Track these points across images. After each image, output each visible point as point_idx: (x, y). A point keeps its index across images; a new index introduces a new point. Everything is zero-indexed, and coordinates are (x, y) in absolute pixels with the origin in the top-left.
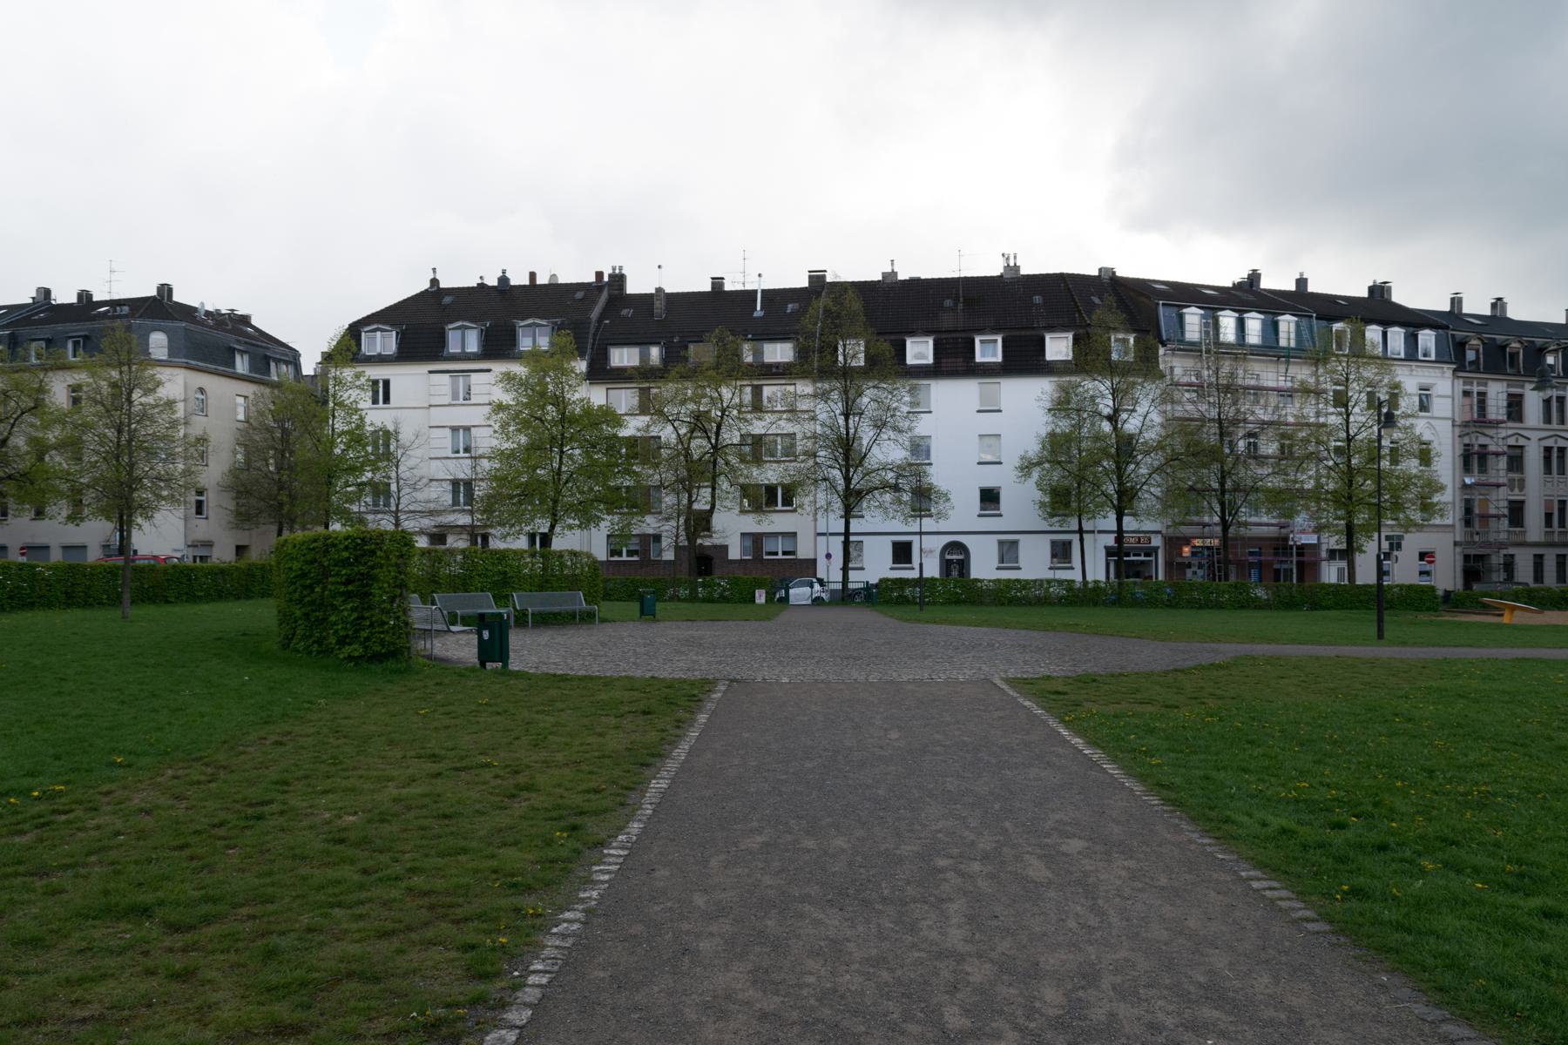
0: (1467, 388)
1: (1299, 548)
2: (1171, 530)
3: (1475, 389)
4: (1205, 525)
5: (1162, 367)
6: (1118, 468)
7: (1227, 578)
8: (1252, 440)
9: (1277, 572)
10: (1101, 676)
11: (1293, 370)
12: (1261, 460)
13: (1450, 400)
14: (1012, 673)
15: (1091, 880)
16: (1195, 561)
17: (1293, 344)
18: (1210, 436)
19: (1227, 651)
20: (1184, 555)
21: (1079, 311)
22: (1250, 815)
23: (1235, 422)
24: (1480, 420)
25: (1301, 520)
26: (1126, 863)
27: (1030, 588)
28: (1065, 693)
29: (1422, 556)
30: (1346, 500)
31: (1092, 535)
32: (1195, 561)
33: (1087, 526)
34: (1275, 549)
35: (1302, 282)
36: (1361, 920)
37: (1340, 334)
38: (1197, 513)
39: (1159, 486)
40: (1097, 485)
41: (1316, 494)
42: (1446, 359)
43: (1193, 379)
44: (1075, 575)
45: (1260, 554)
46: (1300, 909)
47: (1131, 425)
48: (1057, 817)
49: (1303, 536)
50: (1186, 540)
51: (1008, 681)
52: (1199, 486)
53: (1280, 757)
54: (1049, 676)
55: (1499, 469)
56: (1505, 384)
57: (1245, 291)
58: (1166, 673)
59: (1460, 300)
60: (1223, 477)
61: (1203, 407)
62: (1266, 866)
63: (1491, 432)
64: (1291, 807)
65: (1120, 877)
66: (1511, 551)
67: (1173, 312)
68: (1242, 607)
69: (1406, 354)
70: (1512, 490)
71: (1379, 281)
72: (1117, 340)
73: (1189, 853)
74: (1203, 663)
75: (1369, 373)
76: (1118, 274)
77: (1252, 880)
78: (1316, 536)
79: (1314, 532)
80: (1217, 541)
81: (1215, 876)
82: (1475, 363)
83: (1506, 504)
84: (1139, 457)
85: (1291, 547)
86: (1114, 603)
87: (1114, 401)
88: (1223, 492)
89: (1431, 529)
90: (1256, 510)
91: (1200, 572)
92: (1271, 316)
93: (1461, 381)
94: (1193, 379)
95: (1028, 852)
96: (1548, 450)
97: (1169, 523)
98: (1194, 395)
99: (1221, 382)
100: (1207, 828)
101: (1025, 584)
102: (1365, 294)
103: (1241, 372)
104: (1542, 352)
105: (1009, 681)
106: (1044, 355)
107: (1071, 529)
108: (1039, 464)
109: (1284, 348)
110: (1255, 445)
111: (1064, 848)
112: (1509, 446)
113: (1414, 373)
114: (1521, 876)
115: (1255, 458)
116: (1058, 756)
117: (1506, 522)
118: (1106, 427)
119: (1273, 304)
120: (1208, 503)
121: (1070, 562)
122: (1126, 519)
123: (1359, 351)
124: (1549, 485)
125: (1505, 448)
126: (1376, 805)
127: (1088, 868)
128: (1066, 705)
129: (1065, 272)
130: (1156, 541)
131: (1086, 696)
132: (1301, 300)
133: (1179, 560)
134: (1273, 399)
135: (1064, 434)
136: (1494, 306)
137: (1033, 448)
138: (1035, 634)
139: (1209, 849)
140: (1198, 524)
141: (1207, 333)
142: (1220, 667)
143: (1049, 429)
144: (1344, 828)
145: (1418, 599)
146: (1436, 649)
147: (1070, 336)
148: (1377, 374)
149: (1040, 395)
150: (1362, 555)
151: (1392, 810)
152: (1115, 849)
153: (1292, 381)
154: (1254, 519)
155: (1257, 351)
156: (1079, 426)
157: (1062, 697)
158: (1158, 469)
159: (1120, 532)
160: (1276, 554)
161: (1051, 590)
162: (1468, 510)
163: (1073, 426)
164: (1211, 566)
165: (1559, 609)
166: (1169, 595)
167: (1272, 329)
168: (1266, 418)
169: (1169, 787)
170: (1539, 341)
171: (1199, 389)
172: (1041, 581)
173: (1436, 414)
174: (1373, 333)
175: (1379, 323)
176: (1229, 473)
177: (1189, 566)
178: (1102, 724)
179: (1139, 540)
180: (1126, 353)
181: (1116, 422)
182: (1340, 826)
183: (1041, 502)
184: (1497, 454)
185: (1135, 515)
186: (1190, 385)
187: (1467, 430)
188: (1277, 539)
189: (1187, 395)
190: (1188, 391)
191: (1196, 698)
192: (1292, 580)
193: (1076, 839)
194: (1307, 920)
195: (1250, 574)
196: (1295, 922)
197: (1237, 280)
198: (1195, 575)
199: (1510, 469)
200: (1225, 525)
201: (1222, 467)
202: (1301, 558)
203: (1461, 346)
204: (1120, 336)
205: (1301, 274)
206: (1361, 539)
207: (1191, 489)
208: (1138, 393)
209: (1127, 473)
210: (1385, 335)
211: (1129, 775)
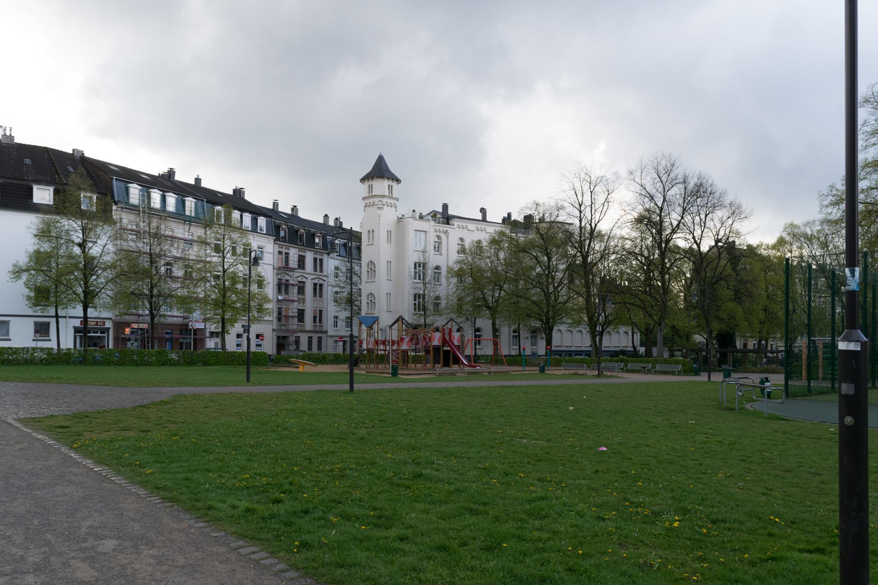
0: (281, 250)
1: (195, 330)
2: (118, 318)
3: (284, 251)
4: (139, 315)
5: (114, 217)
6: (86, 277)
7: (152, 348)
8: (169, 267)
9: (182, 344)
10: (91, 413)
11: (193, 229)
12: (174, 279)
13: (272, 255)
14: (22, 414)
15: (129, 571)
16: (133, 337)
17: (193, 215)
18: (144, 262)
19: (167, 392)
20: (126, 333)
21: (59, 174)
22: (224, 502)
23: (159, 256)
24: (285, 268)
25: (197, 315)
26: (151, 552)
27: (19, 353)
28: (68, 427)
29: (258, 336)
30: (222, 304)
31: (64, 319)
32: (133, 337)
33: (61, 313)
34: (181, 331)
35: (198, 180)
36: (314, 565)
37: (219, 212)
38: (136, 308)
39: (112, 290)
40: (69, 287)
41: (205, 301)
42: (271, 233)
43: (134, 227)
44: (53, 345)
45: (172, 333)
46: (277, 563)
47: (95, 251)
48: (88, 523)
49: (197, 324)
50: (128, 324)
51: (19, 420)
52: (137, 292)
53: (226, 459)
54: (52, 415)
55: (294, 291)
56: (297, 249)
57: (166, 180)
58: (134, 408)
59: (277, 204)
60: (152, 288)
61: (140, 245)
62: (246, 537)
63: (291, 274)
64: (245, 492)
65: (150, 565)
66: (298, 334)
67: (122, 185)
68: (163, 365)
69: (252, 228)
70: (299, 304)
71: (239, 187)
72: (84, 196)
73: (192, 536)
74: (155, 400)
75: (235, 236)
76: (86, 155)
77: (239, 548)
78: (203, 324)
79: (203, 322)
80: (147, 325)
81: (215, 550)
82: (284, 237)
83: (296, 311)
84: (100, 272)
85: (190, 330)
86: (80, 363)
87: (83, 234)
88: (152, 296)
89: (265, 322)
90: (171, 308)
91: (136, 344)
92: (181, 197)
93: (278, 246)
94: (134, 227)
95: (73, 558)
96: (315, 284)
97: (117, 314)
98: (134, 237)
99: (151, 231)
100: (199, 515)
101: (15, 351)
102: (231, 193)
103: (163, 226)
104: (313, 236)
105: (23, 421)
106: (32, 199)
107: (49, 314)
108: (27, 270)
109: (188, 216)
110: (170, 270)
111: (100, 549)
112: (299, 282)
113: (256, 239)
114: (380, 517)
115: (171, 277)
116: (75, 474)
117: (296, 319)
118: (77, 250)
119: (183, 190)
120: (143, 302)
121: (48, 336)
122: (90, 310)
123: (228, 224)
124: (315, 302)
125: (297, 282)
126: (291, 484)
127: (124, 561)
128: (72, 436)
129: (49, 147)
130: (108, 324)
131: (84, 428)
132: (196, 190)
133: (123, 336)
134: (182, 245)
135: (46, 253)
136: (293, 209)
137: (23, 260)
138: (31, 385)
139: (205, 530)
140: (135, 315)
141: (144, 201)
142: (167, 403)
143: (35, 248)
144: (280, 502)
145: (261, 360)
146: (277, 387)
147: (52, 189)
148: (239, 237)
149: (30, 224)
150: (228, 335)
151: (301, 486)
152: (140, 542)
153: (192, 235)
154: (169, 313)
155: (171, 215)
156: (57, 248)
157: (66, 430)
158: (112, 279)
159: (85, 317)
160: (181, 334)
161: (36, 354)
162: (280, 313)
163: (53, 248)
164: (143, 341)
165: (322, 364)
166: (118, 357)
167: (181, 204)
168: (178, 255)
169: (164, 489)
170: (313, 230)
171: (138, 233)
172: (28, 348)
173: (265, 262)
174: (236, 214)
175: (239, 210)
176: (156, 285)
177: (129, 340)
178: (102, 447)
179: (97, 323)
180: (92, 205)
181: (85, 248)
182: (278, 501)
183: (28, 296)
184: (293, 285)
185: (95, 307)
186: (132, 230)
187: (280, 272)
188: (182, 325)
189: (130, 237)
190: (131, 234)
191: (160, 424)
192: (190, 348)
193: (108, 539)
194: (284, 571)
195: (166, 346)
196: (276, 574)
197: (161, 173)
198: (132, 345)
199: (299, 293)
200: (153, 317)
201: (151, 281)
202: (195, 337)
203: (278, 228)
204: (88, 194)
205: (198, 176)
206: (228, 327)
207: (132, 293)
208: (98, 230)
209: (91, 281)
210: (241, 216)
211: (134, 483)
